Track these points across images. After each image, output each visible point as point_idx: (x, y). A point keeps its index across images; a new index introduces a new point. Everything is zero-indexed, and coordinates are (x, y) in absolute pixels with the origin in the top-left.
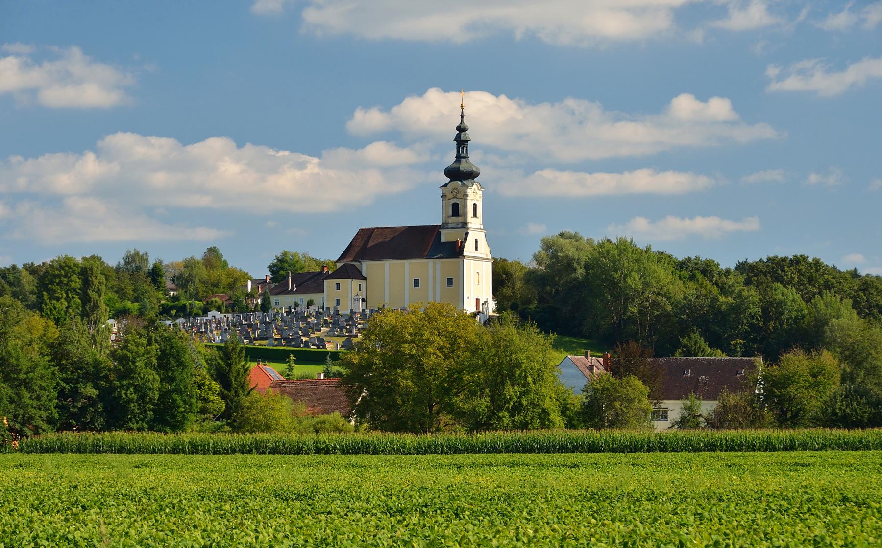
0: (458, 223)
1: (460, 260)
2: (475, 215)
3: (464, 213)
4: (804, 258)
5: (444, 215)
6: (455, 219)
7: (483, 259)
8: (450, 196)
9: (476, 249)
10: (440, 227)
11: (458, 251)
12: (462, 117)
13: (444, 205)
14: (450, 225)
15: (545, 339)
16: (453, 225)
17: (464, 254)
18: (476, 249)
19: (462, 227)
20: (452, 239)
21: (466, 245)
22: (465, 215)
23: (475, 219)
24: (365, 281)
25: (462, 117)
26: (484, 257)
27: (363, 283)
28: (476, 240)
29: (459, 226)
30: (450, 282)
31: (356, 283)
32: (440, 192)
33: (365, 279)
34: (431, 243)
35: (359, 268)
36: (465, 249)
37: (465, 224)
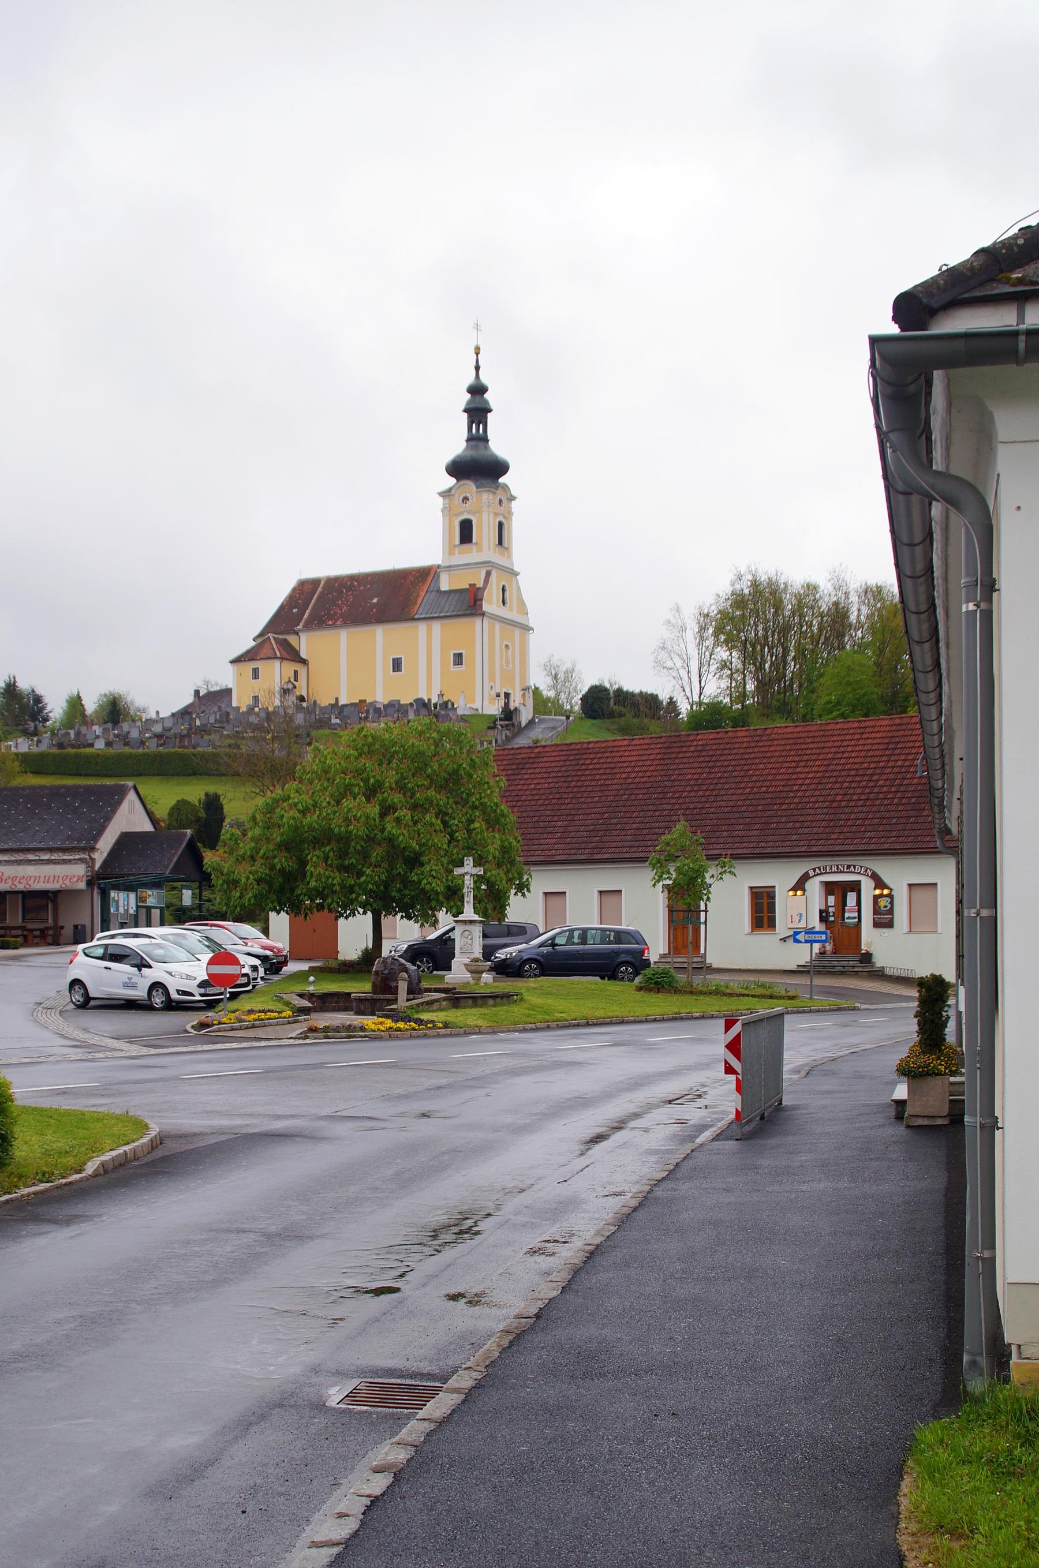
12: (477, 368)
25: (477, 368)
27: (302, 670)
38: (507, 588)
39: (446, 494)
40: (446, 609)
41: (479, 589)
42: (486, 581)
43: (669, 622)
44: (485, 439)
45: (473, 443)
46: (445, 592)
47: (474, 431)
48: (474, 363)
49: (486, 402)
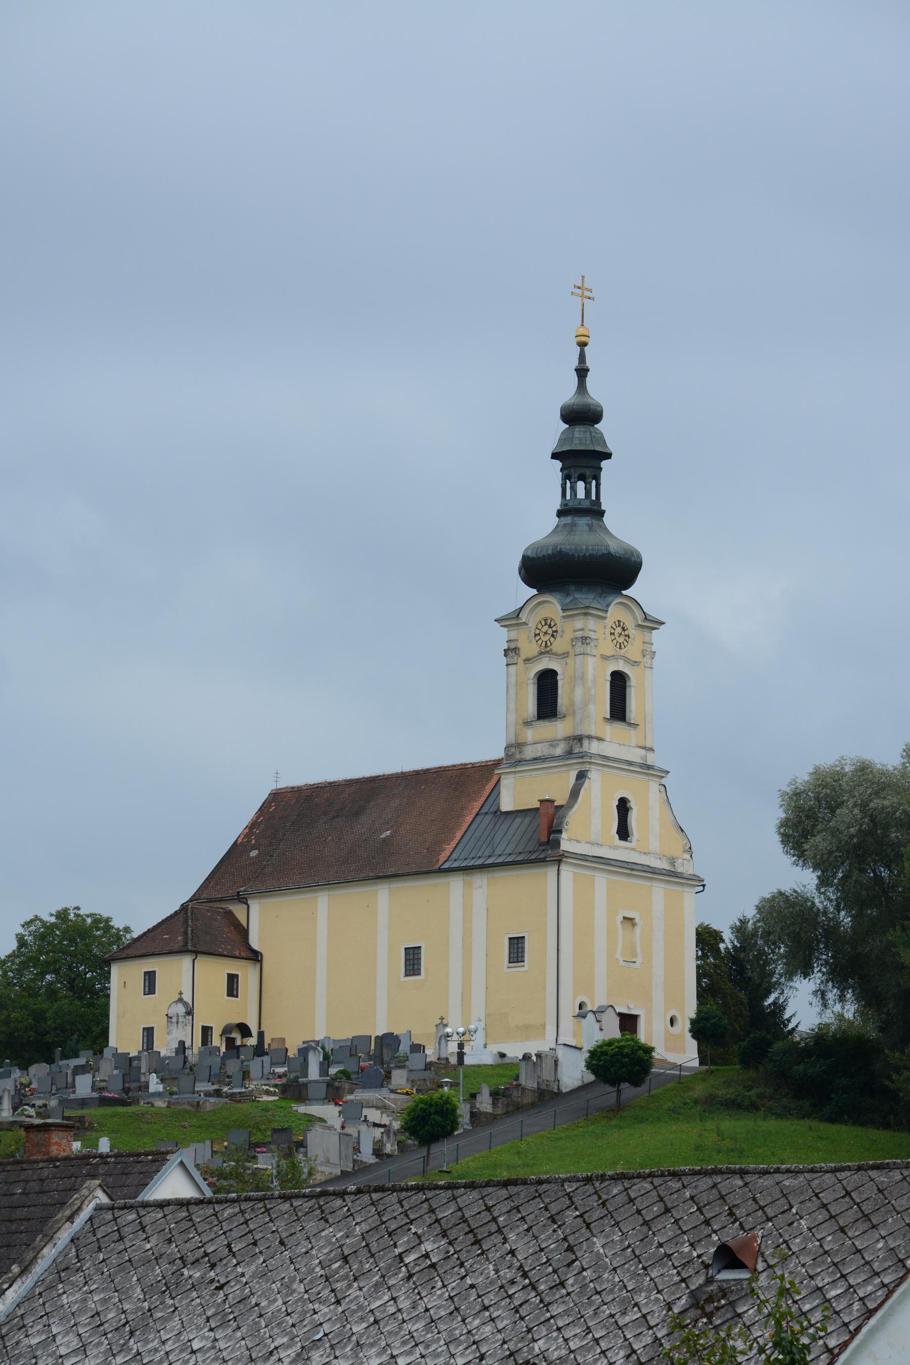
0: (553, 743)
4: (784, 824)
5: (512, 718)
7: (654, 871)
8: (529, 647)
9: (624, 833)
10: (497, 763)
12: (582, 372)
13: (513, 680)
14: (529, 752)
17: (565, 846)
23: (618, 726)
25: (582, 372)
27: (247, 974)
32: (501, 637)
35: (242, 918)
38: (632, 804)
39: (512, 620)
40: (498, 851)
41: (560, 807)
42: (575, 793)
43: (184, 1042)
44: (595, 511)
45: (568, 520)
46: (508, 813)
47: (568, 497)
48: (575, 363)
49: (602, 440)
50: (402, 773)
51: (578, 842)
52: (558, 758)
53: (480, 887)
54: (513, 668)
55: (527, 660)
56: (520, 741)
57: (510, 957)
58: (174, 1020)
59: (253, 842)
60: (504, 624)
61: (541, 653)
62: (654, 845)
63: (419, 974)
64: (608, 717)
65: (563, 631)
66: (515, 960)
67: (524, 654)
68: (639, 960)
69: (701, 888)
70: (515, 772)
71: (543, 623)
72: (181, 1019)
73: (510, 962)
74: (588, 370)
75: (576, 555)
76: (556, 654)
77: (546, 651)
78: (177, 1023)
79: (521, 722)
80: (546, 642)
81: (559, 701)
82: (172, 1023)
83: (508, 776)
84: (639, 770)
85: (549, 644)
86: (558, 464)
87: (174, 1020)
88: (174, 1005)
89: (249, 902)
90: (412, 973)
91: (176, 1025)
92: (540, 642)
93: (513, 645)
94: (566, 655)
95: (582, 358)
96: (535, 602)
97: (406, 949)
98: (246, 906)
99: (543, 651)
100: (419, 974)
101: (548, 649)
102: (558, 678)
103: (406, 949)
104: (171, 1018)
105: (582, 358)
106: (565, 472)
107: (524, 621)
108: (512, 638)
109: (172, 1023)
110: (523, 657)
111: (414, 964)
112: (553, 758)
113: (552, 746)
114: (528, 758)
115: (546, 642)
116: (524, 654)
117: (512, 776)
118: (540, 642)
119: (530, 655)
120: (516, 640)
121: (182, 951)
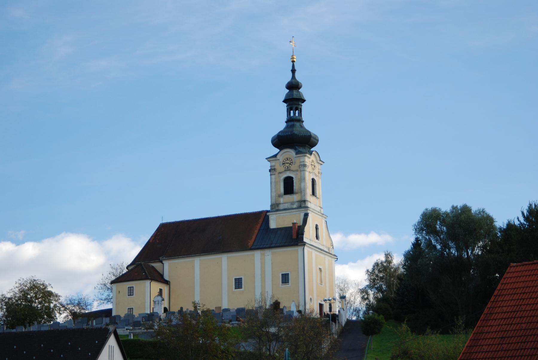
0: (292, 203)
1: (300, 249)
2: (314, 193)
3: (300, 189)
5: (274, 194)
6: (288, 198)
10: (268, 211)
11: (294, 237)
12: (293, 71)
13: (273, 180)
14: (281, 207)
15: (335, 334)
16: (286, 206)
18: (317, 237)
19: (300, 207)
20: (288, 223)
21: (306, 229)
22: (302, 191)
23: (314, 198)
24: (168, 286)
25: (293, 71)
26: (327, 250)
27: (165, 289)
28: (317, 226)
29: (295, 206)
30: (285, 278)
31: (156, 286)
32: (268, 165)
33: (167, 283)
34: (256, 231)
36: (304, 236)
37: (302, 204)
45: (290, 123)
48: (291, 68)
50: (218, 216)
51: (307, 239)
52: (295, 208)
53: (268, 255)
54: (273, 176)
55: (280, 173)
56: (277, 202)
57: (282, 281)
58: (157, 302)
59: (158, 241)
60: (268, 160)
61: (285, 170)
62: (324, 243)
63: (242, 288)
64: (311, 194)
65: (295, 162)
66: (284, 282)
67: (278, 171)
68: (323, 284)
69: (336, 259)
70: (276, 214)
71: (286, 159)
72: (160, 302)
73: (282, 283)
74: (296, 71)
75: (300, 135)
76: (292, 171)
77: (288, 169)
78: (158, 304)
79: (277, 195)
80: (288, 167)
81: (294, 188)
82: (156, 304)
83: (273, 215)
84: (320, 214)
85: (289, 167)
86: (285, 105)
87: (157, 302)
88: (156, 297)
89: (164, 262)
90: (238, 287)
91: (157, 304)
92: (285, 167)
93: (273, 168)
94: (297, 171)
95: (293, 66)
96: (282, 153)
97: (235, 279)
98: (162, 264)
99: (286, 169)
100: (242, 288)
101: (288, 169)
102: (294, 179)
103: (235, 279)
104: (155, 302)
105: (293, 66)
106: (290, 106)
107: (278, 158)
108: (272, 165)
109: (156, 304)
110: (278, 172)
111: (239, 285)
112: (293, 209)
113: (292, 204)
114: (281, 209)
115: (288, 167)
116: (278, 171)
117: (275, 215)
118: (285, 167)
119: (280, 171)
120: (275, 166)
121: (146, 278)
